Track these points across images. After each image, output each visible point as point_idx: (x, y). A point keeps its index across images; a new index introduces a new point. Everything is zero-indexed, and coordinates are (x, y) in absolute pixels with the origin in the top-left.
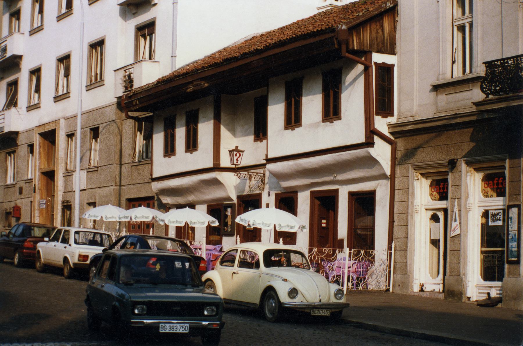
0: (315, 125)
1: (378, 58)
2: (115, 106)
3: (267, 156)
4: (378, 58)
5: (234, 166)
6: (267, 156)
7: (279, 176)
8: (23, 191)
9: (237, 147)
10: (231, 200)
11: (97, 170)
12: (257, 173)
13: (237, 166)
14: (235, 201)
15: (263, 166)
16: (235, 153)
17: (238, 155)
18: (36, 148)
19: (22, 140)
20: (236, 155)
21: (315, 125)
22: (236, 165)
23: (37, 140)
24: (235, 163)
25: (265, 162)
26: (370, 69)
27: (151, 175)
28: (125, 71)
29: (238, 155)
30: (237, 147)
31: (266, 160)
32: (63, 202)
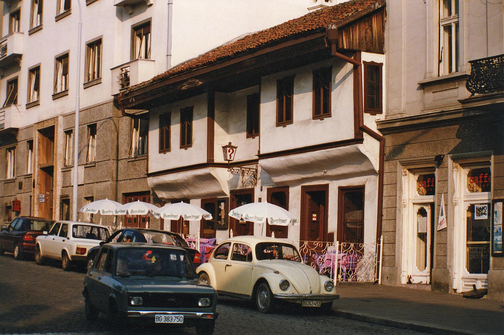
0: (305, 122)
1: (366, 57)
2: (112, 103)
3: (259, 152)
4: (366, 57)
5: (227, 162)
6: (259, 152)
7: (271, 172)
8: (23, 186)
9: (230, 143)
10: (224, 194)
11: (95, 166)
12: (250, 169)
13: (230, 162)
14: (229, 195)
15: (255, 161)
16: (228, 149)
17: (231, 151)
18: (36, 145)
19: (22, 137)
20: (229, 151)
21: (305, 122)
22: (229, 161)
23: (36, 137)
24: (228, 158)
25: (257, 157)
26: (359, 67)
27: (147, 171)
28: (122, 69)
29: (231, 151)
30: (230, 143)
31: (258, 156)
32: (62, 197)
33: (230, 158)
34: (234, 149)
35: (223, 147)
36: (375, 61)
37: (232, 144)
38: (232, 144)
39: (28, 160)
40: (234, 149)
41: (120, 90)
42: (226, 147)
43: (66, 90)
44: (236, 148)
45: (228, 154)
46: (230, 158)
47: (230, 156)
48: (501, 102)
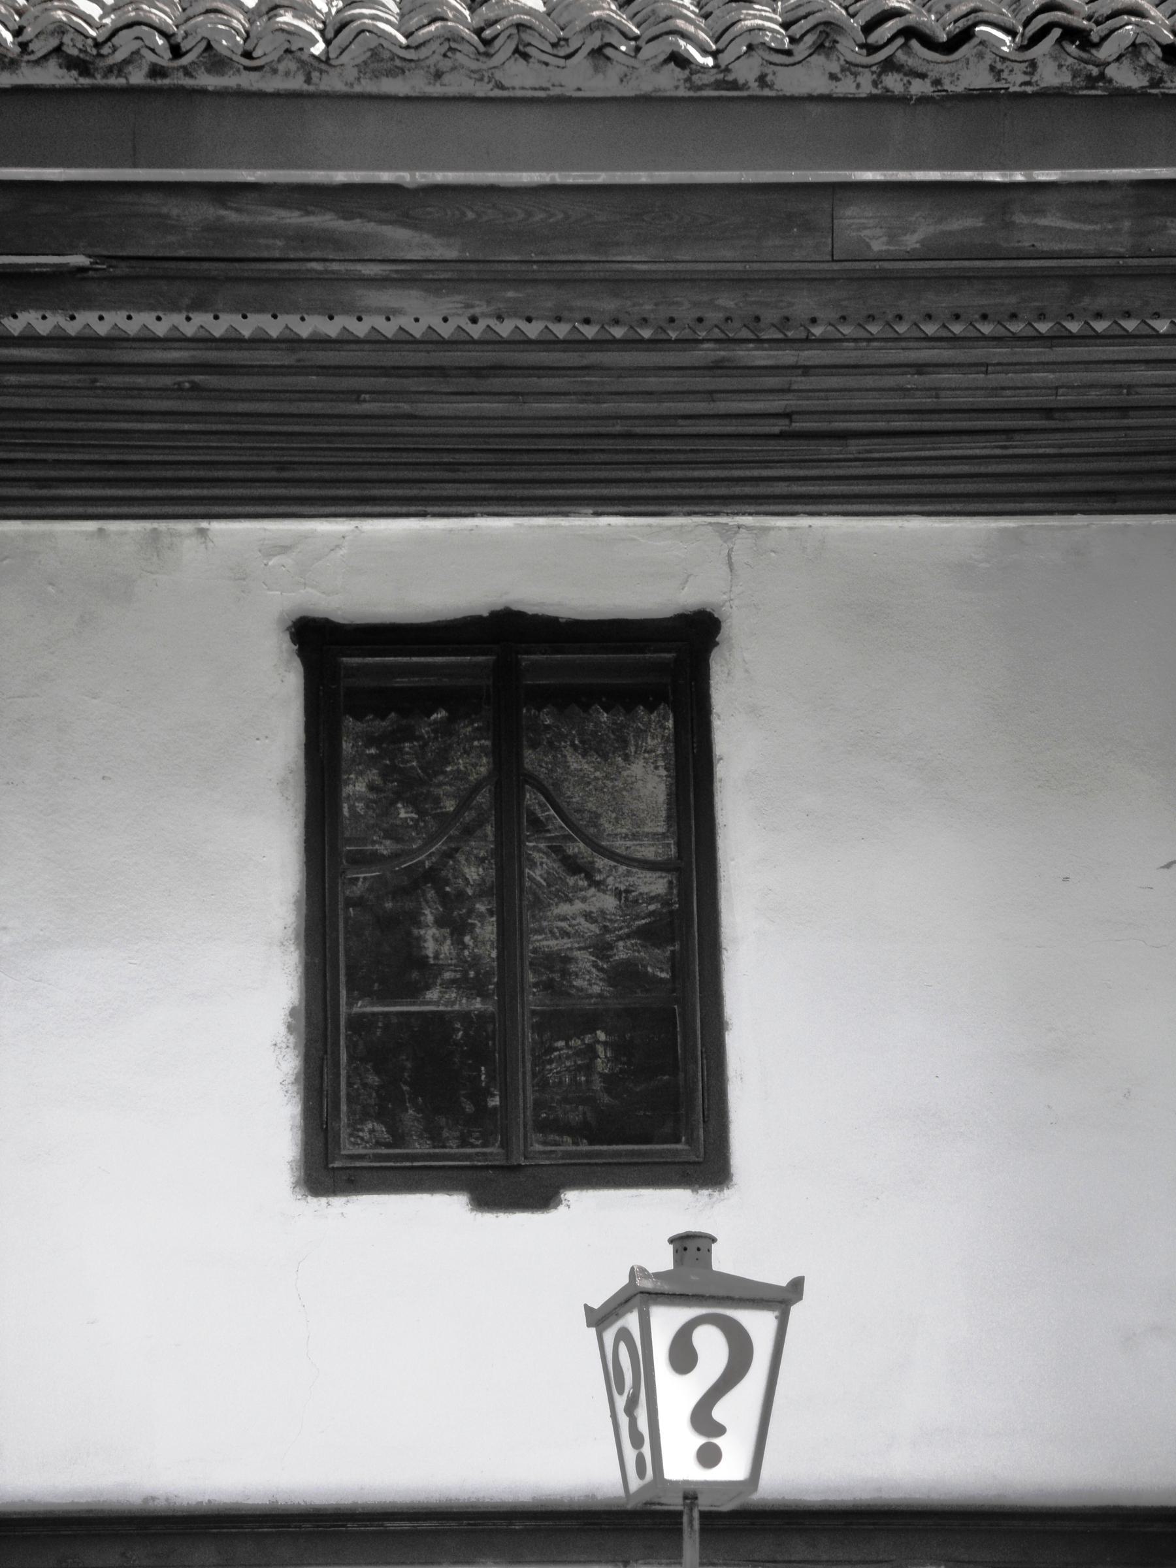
16: (666, 1322)
17: (711, 1346)
20: (684, 1357)
29: (711, 1346)
33: (709, 1456)
34: (759, 1324)
35: (599, 1318)
36: (448, 1209)
37: (723, 1261)
38: (723, 1261)
39: (493, 189)
40: (759, 1324)
41: (327, 72)
42: (639, 1295)
43: (492, 55)
44: (781, 1299)
45: (676, 1395)
46: (709, 1456)
47: (703, 1418)
48: (400, 659)
